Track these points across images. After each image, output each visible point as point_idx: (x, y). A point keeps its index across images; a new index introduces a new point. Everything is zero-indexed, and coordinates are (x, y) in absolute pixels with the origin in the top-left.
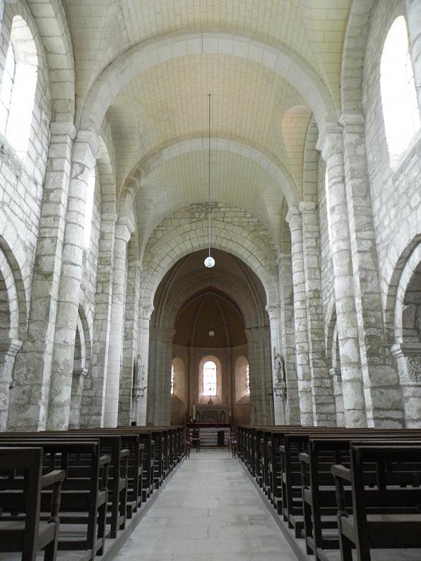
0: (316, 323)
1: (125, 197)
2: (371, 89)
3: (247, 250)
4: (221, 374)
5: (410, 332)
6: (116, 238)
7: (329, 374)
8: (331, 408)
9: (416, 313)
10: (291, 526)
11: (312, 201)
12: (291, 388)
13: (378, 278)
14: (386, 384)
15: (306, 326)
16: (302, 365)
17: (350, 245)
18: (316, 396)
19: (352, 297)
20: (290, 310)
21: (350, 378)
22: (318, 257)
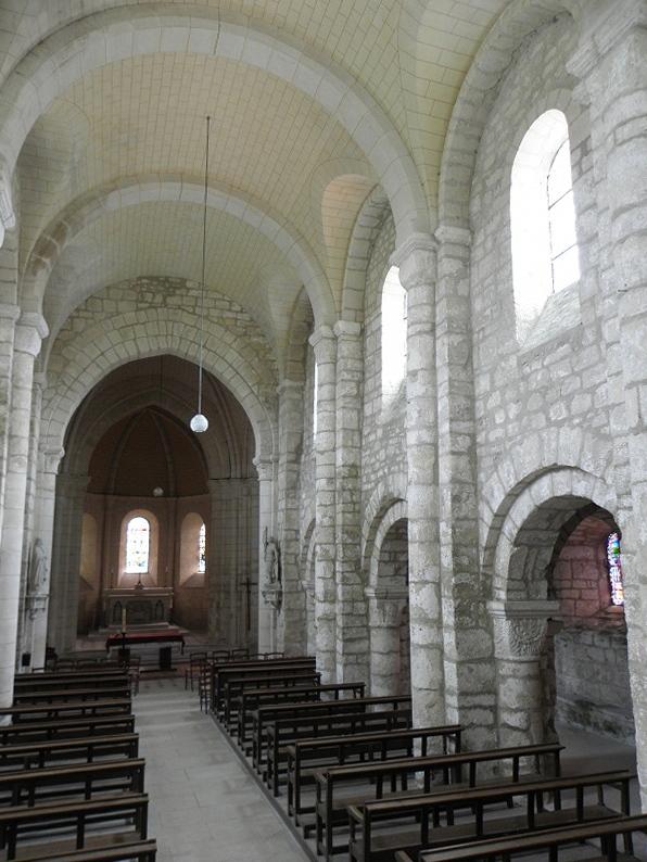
1: (35, 274)
2: (488, 196)
3: (230, 365)
4: (157, 538)
5: (517, 585)
6: (15, 351)
7: (364, 595)
8: (363, 646)
9: (527, 558)
10: (243, 749)
11: (356, 321)
12: (290, 592)
13: (476, 496)
15: (333, 518)
17: (437, 436)
18: (343, 628)
19: (435, 520)
22: (359, 413)
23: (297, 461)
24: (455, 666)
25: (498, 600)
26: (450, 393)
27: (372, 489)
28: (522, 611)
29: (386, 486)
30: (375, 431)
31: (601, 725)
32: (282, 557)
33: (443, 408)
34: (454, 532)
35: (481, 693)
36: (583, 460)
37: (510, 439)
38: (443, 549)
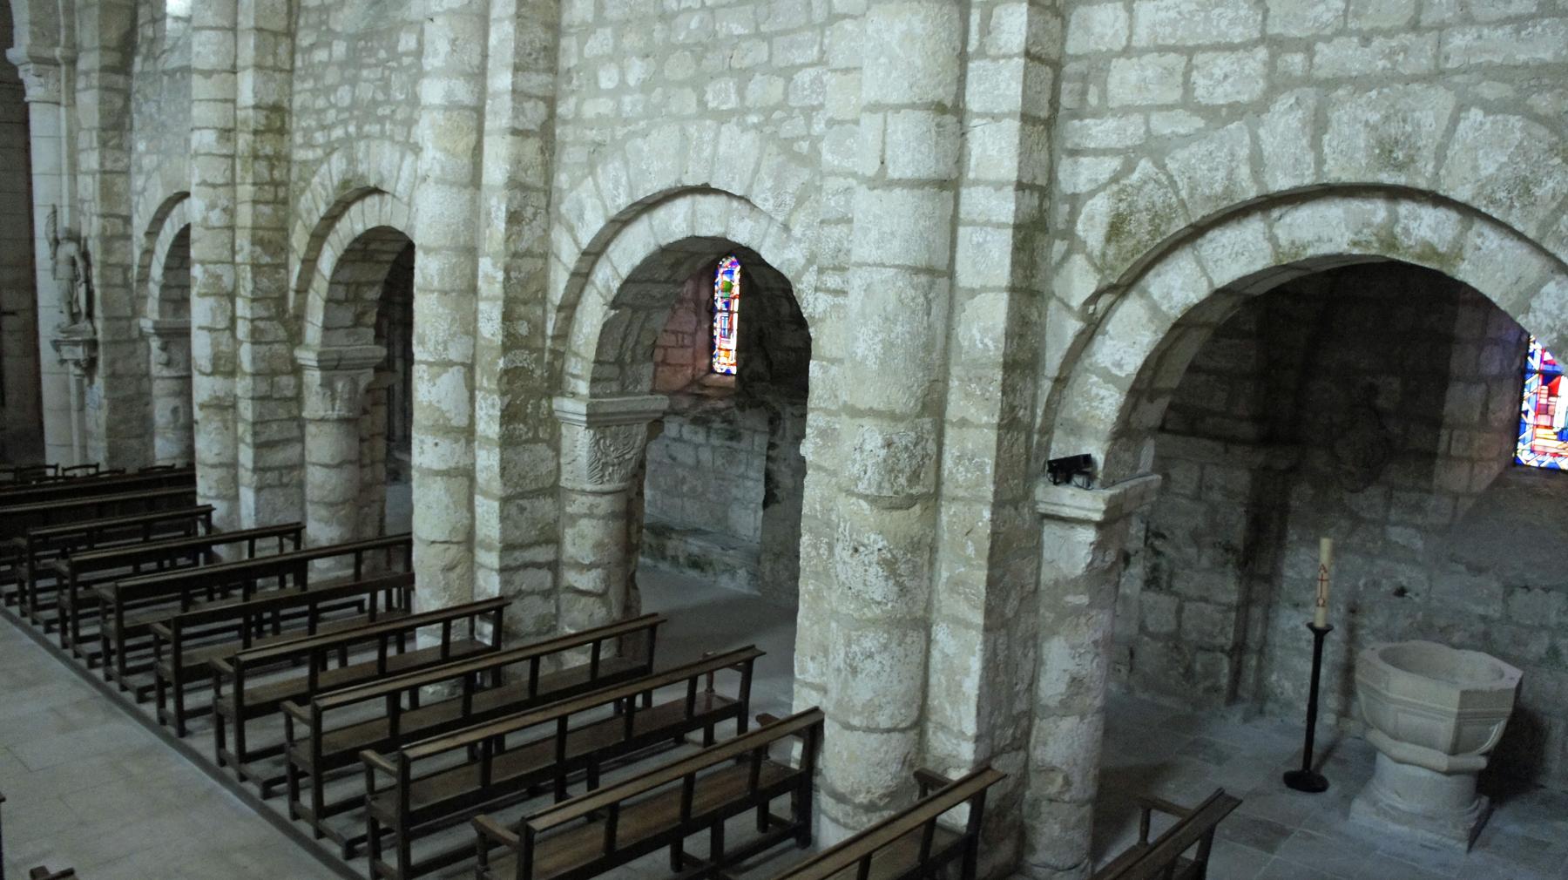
0: (267, 210)
7: (293, 360)
12: (115, 342)
14: (534, 486)
16: (210, 330)
17: (482, 94)
18: (254, 424)
19: (471, 252)
20: (118, 91)
21: (443, 467)
23: (123, 68)
24: (496, 504)
25: (574, 395)
26: (518, 16)
27: (319, 162)
28: (613, 414)
29: (352, 161)
30: (329, 45)
31: (681, 560)
32: (95, 271)
33: (501, 41)
34: (507, 278)
35: (537, 543)
36: (756, 189)
37: (626, 122)
38: (482, 306)
